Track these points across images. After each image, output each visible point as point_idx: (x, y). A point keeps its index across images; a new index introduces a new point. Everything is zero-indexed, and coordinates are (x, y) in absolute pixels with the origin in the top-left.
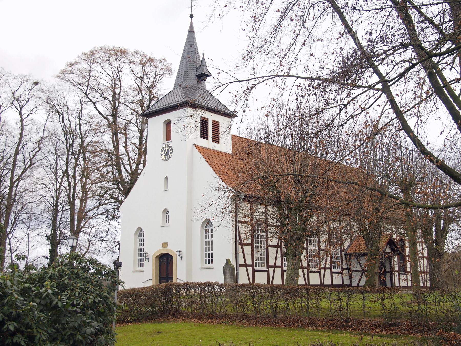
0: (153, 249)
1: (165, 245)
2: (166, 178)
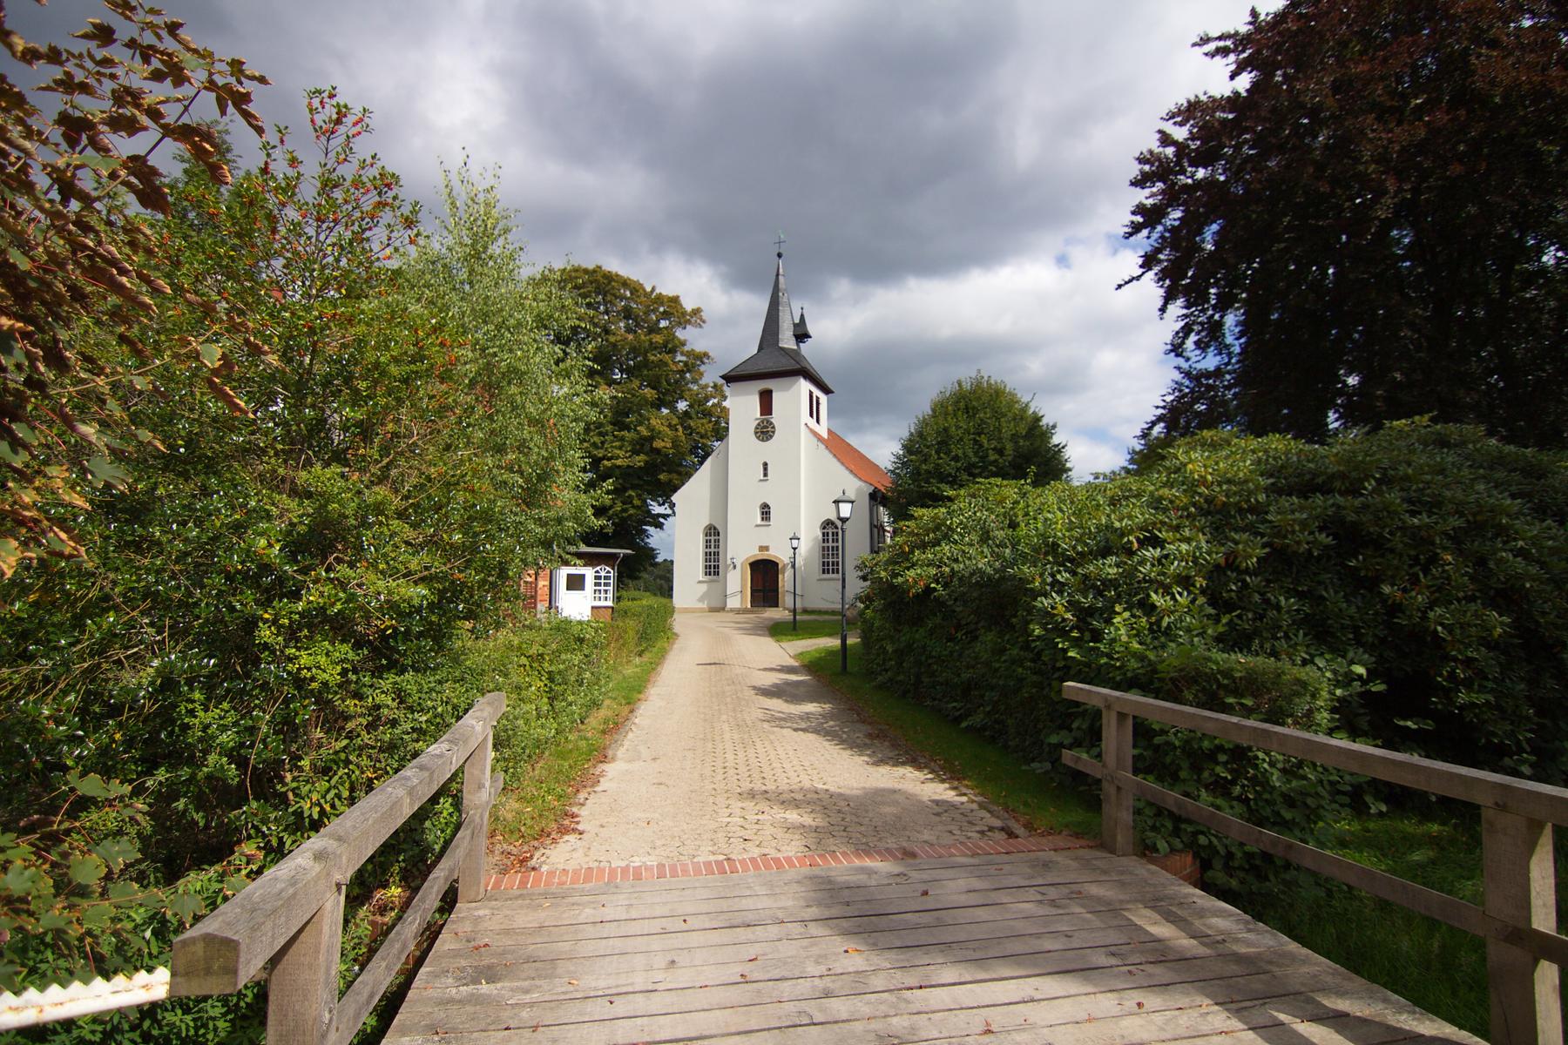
0: (741, 548)
1: (764, 548)
2: (765, 465)
